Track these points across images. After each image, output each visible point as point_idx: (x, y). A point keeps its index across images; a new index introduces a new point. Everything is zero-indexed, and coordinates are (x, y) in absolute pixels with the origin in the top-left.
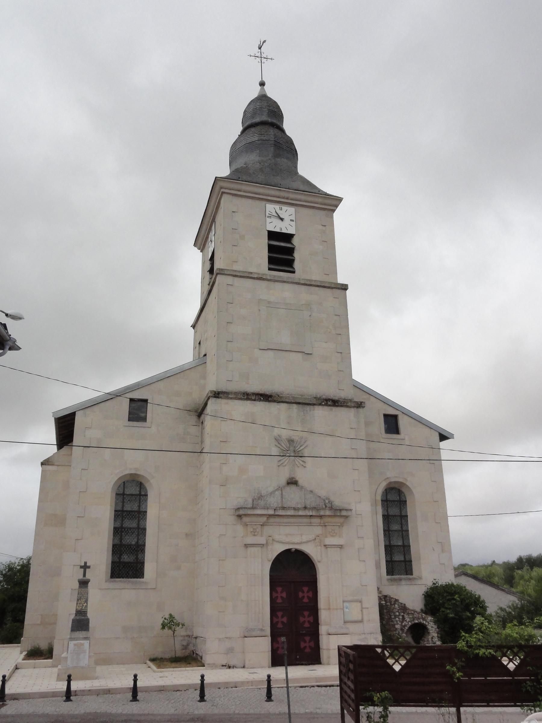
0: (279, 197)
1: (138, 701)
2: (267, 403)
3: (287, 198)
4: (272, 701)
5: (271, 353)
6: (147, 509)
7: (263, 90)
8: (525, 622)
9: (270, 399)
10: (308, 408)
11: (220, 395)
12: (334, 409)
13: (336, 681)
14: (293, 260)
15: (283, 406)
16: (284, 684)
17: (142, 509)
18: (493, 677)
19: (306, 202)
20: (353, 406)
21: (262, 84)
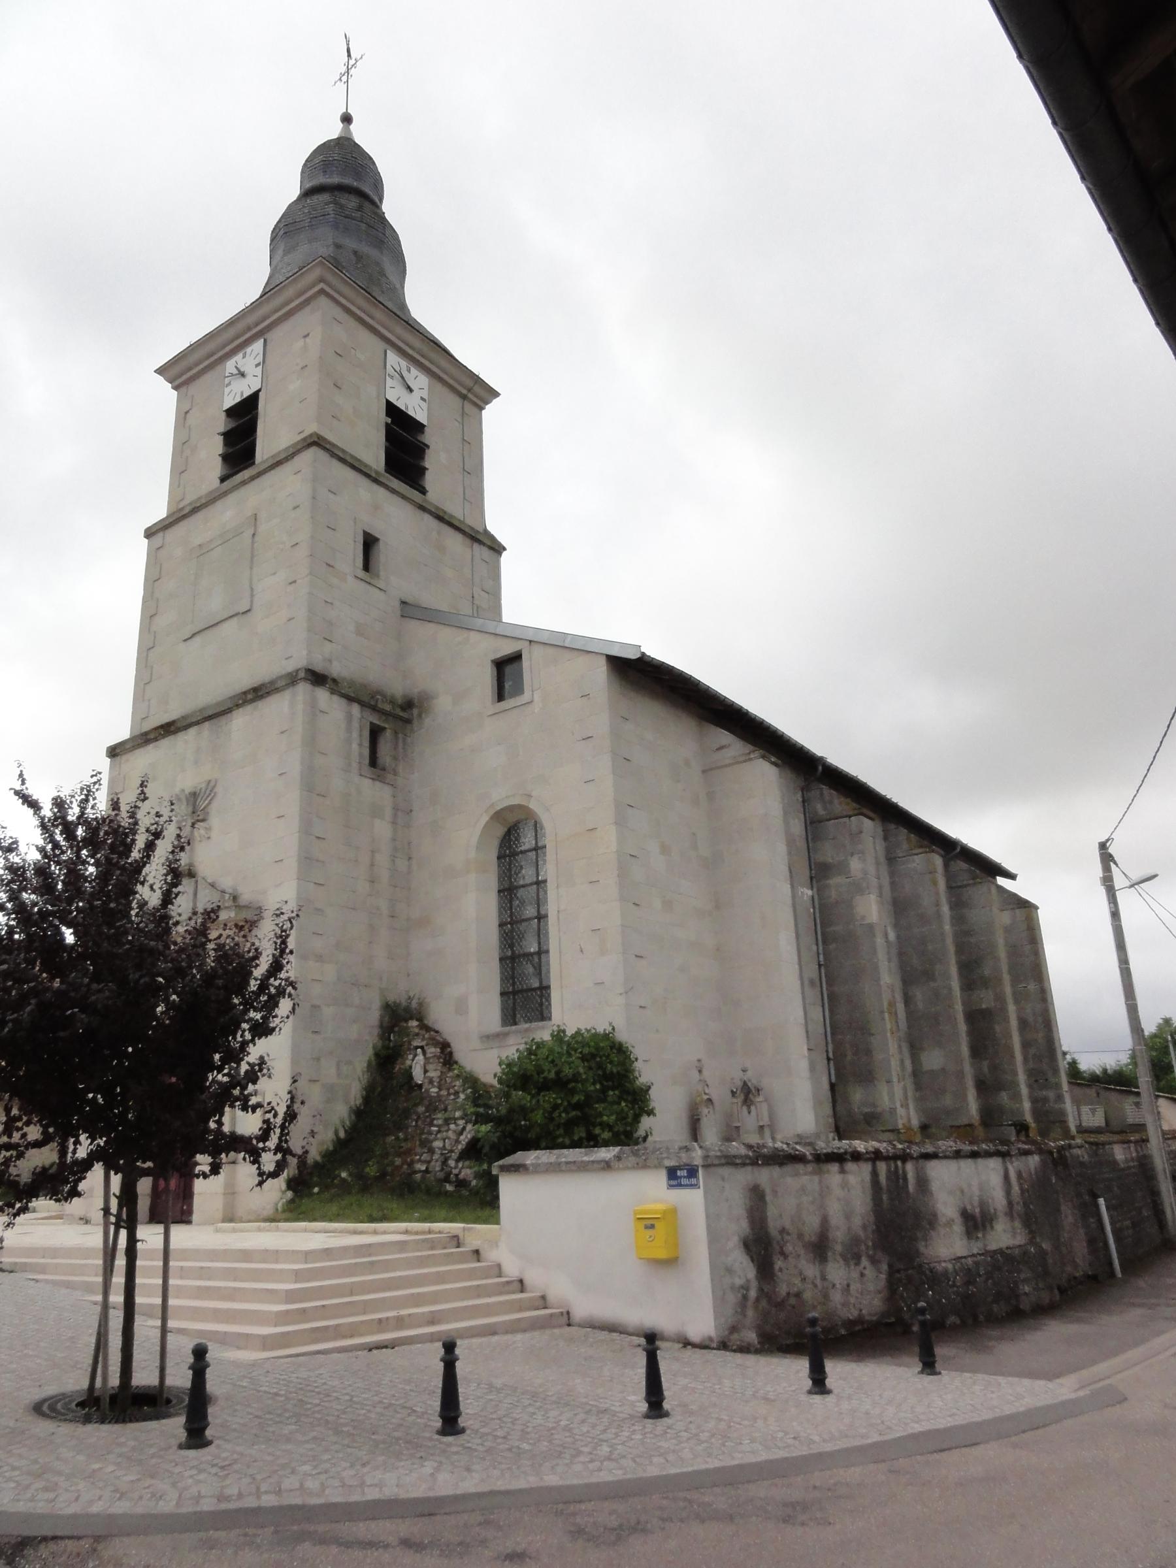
0: (237, 337)
1: (828, 1392)
2: (172, 738)
3: (249, 329)
4: (828, 1392)
5: (198, 639)
6: (550, 981)
7: (346, 129)
8: (427, 1114)
9: (172, 728)
10: (223, 719)
11: (118, 751)
12: (260, 704)
13: (143, 1267)
14: (484, 409)
15: (192, 731)
16: (96, 1275)
17: (545, 984)
18: (332, 1267)
19: (276, 311)
20: (284, 684)
21: (347, 119)
